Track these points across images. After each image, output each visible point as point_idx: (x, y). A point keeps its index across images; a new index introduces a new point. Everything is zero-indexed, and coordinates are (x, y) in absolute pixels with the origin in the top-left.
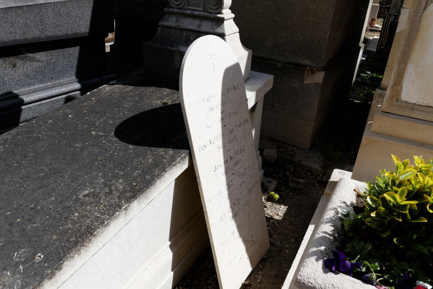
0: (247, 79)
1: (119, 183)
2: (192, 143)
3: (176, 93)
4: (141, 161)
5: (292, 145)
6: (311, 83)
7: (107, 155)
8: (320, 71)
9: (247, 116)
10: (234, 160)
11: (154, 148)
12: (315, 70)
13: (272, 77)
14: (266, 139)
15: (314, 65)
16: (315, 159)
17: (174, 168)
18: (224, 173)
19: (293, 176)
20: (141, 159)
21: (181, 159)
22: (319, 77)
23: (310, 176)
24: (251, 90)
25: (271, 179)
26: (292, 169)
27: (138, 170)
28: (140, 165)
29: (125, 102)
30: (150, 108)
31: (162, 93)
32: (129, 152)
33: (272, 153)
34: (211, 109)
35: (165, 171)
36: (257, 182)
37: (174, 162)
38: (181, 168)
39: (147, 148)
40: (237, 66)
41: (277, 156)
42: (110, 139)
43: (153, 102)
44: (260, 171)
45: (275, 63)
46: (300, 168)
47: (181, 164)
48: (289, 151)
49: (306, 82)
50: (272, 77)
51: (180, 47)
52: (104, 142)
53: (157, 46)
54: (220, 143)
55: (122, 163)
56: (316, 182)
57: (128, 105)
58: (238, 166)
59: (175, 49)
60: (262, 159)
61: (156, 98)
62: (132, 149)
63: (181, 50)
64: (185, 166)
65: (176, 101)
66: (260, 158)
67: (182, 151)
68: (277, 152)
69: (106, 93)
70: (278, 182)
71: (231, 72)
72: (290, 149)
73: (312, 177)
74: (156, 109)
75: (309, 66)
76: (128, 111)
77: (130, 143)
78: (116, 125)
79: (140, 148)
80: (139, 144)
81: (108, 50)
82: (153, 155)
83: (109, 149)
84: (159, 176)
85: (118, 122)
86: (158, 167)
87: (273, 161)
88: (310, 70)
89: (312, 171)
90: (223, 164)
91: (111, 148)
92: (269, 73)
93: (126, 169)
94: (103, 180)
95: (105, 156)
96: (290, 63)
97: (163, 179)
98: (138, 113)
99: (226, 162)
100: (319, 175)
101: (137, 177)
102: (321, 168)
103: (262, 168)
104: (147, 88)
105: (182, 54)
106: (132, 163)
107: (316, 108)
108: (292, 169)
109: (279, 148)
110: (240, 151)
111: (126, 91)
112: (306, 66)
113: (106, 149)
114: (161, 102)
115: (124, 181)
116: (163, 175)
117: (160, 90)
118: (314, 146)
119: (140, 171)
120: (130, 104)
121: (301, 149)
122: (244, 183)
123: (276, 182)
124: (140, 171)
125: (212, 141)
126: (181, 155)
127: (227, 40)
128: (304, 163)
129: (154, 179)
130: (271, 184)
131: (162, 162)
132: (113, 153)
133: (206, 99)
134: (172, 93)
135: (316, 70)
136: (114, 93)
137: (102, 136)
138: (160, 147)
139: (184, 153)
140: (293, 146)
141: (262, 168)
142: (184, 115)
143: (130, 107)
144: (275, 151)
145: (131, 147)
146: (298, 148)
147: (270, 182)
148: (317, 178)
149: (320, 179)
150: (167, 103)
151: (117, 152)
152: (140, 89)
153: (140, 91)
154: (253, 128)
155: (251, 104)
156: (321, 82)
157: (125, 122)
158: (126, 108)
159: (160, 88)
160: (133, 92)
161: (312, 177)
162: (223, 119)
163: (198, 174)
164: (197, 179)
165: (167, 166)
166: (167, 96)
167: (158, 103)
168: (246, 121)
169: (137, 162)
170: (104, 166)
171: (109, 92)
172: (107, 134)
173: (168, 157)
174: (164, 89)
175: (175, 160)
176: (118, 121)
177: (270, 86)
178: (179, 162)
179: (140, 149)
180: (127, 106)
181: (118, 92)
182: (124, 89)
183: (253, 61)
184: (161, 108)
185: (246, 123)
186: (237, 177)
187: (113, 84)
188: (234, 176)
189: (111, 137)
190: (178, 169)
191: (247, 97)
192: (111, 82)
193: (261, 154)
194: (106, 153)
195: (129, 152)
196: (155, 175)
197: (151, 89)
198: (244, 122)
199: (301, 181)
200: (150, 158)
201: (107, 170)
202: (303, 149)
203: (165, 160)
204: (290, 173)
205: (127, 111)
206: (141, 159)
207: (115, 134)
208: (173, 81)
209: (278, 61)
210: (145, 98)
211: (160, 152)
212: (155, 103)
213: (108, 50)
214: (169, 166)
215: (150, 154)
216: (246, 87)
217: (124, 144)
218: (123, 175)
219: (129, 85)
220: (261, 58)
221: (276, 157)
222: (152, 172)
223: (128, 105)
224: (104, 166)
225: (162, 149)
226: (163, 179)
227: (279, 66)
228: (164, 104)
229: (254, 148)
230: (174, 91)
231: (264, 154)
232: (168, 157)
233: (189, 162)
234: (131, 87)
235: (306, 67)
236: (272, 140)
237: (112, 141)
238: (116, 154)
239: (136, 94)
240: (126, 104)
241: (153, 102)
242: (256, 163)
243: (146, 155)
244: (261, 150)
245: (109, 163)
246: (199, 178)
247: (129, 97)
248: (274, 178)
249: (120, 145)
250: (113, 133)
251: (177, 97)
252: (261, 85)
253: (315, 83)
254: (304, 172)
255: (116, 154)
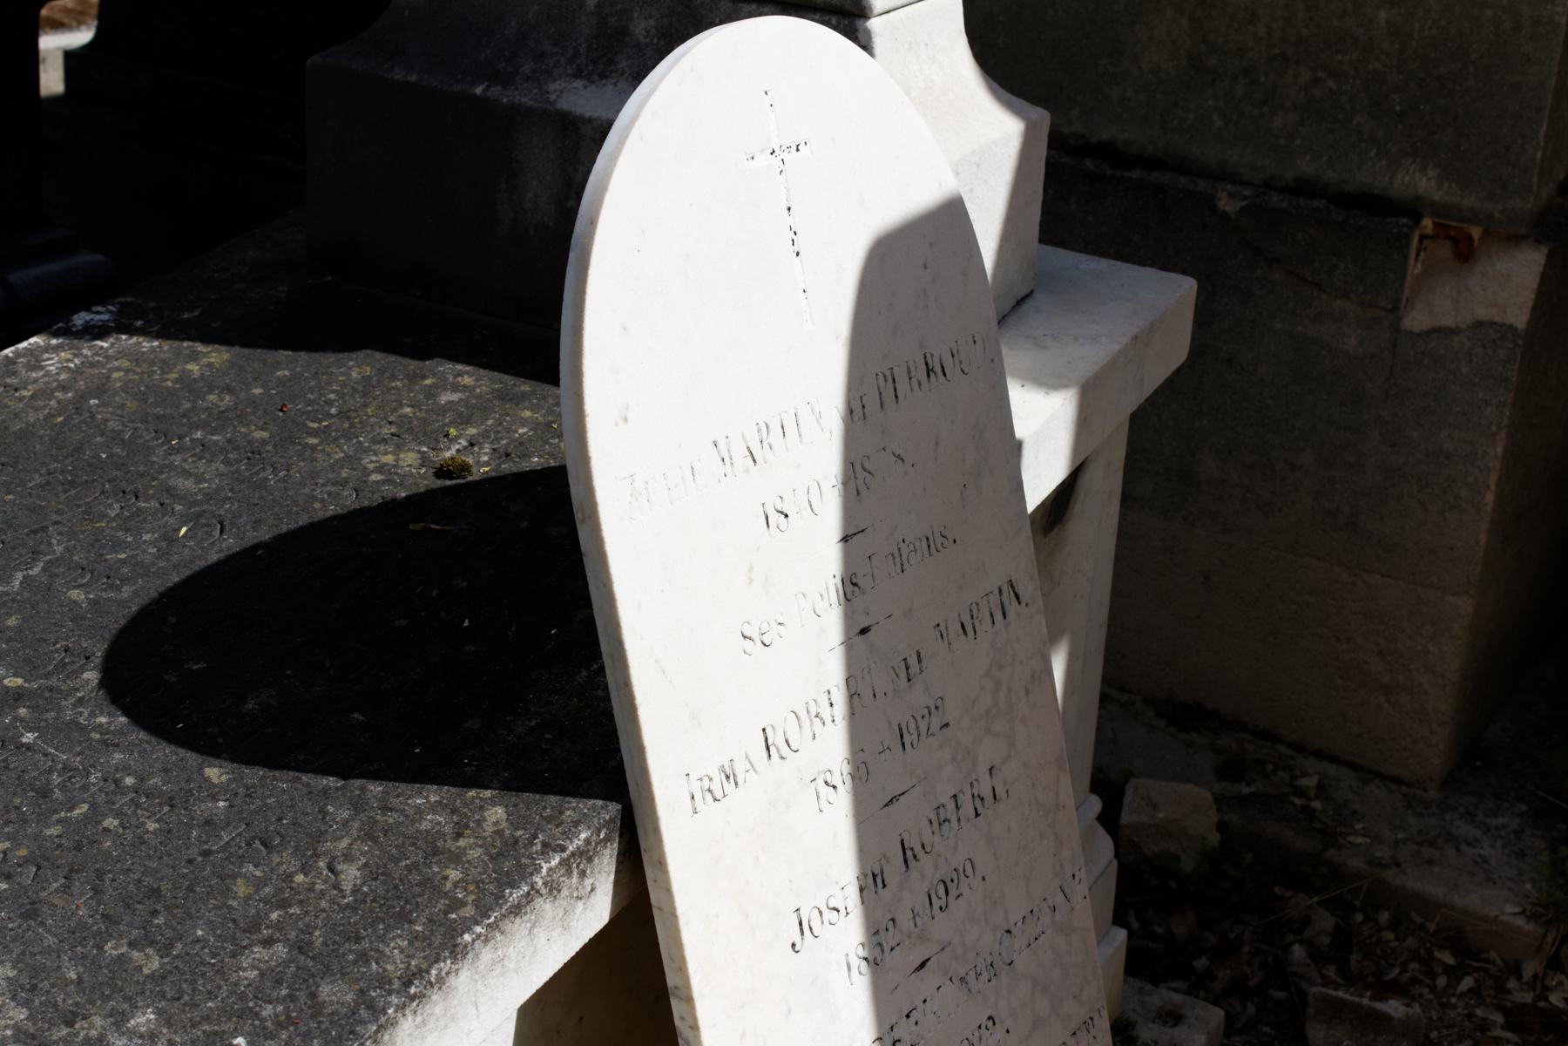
0: (1017, 303)
1: (132, 1034)
2: (640, 750)
3: (524, 397)
4: (288, 877)
5: (1320, 755)
6: (1447, 321)
7: (54, 831)
8: (1515, 240)
9: (1016, 558)
10: (928, 870)
11: (376, 788)
12: (1476, 233)
13: (1179, 291)
14: (1146, 710)
15: (1470, 201)
16: (1486, 851)
17: (518, 927)
18: (856, 963)
19: (1331, 971)
20: (285, 861)
21: (565, 863)
22: (1509, 285)
23: (1455, 974)
24: (1047, 381)
25: (1178, 998)
26: (1325, 922)
27: (268, 943)
28: (283, 904)
29: (177, 460)
30: (350, 501)
31: (431, 394)
32: (203, 809)
33: (1183, 806)
34: (775, 518)
35: (457, 952)
36: (1088, 1024)
37: (514, 885)
38: (557, 930)
39: (331, 782)
40: (949, 218)
41: (1222, 827)
42: (68, 715)
43: (369, 461)
44: (1102, 938)
45: (1201, 185)
46: (1384, 917)
47: (562, 902)
48: (1300, 792)
49: (1416, 320)
50: (1179, 291)
51: (555, 86)
52: (29, 737)
53: (398, 75)
54: (830, 748)
55: (155, 893)
56: (1499, 1018)
57: (197, 477)
58: (958, 908)
59: (522, 96)
60: (1117, 856)
61: (396, 428)
62: (225, 788)
63: (564, 104)
64: (591, 912)
65: (526, 456)
66: (1105, 845)
67: (575, 807)
68: (1219, 800)
69: (46, 393)
70: (1229, 1018)
71: (911, 267)
72: (1310, 782)
73: (1467, 982)
74: (391, 507)
75: (1438, 210)
76: (195, 519)
77: (211, 749)
78: (116, 621)
79: (282, 781)
80: (274, 759)
81: (52, 81)
82: (369, 836)
83: (63, 788)
84: (414, 986)
85: (132, 596)
86: (404, 918)
87: (1188, 864)
88: (1441, 231)
89: (1464, 943)
90: (850, 897)
91: (78, 782)
92: (1164, 262)
93: (180, 937)
94: (21, 1014)
95: (36, 837)
96: (1305, 188)
97: (437, 1005)
98: (265, 534)
99: (872, 882)
100: (1516, 970)
101: (260, 995)
102: (1533, 917)
103: (1119, 919)
104: (328, 359)
105: (582, 142)
106: (227, 892)
107: (1490, 498)
108: (1325, 922)
109: (1230, 769)
110: (966, 801)
111: (184, 377)
112: (1412, 210)
113: (45, 793)
114: (424, 461)
115: (166, 1019)
116: (441, 981)
117: (413, 378)
118: (1477, 762)
119: (281, 950)
120: (213, 472)
121: (1384, 778)
122: (999, 1033)
123: (1219, 1013)
124: (281, 950)
125: (776, 739)
126: (569, 835)
127: (878, 43)
128: (1413, 880)
129: (376, 1011)
130: (1179, 1032)
131: (432, 887)
132: (94, 816)
133: (739, 453)
134: (502, 396)
135: (1486, 233)
136: (100, 390)
137: (18, 696)
138: (420, 775)
139: (587, 823)
140: (1333, 759)
141: (1119, 919)
142: (588, 562)
143: (208, 496)
144: (1202, 795)
145: (215, 773)
146: (1367, 773)
147: (1173, 1017)
148: (1502, 990)
149: (1528, 997)
150: (465, 468)
151: (119, 814)
152: (277, 365)
153: (282, 382)
154: (1053, 638)
155: (1041, 477)
156: (1519, 317)
157: (172, 598)
158: (182, 498)
159: (414, 365)
160: (229, 390)
161: (1467, 982)
162: (851, 586)
163: (682, 969)
164: (676, 1007)
165: (469, 911)
166: (463, 421)
167: (403, 467)
168: (1007, 595)
169: (259, 884)
170: (31, 913)
171: (64, 388)
172: (53, 682)
173: (475, 854)
174: (446, 368)
175: (523, 873)
176: (127, 591)
177: (1174, 351)
178: (553, 889)
179: (280, 788)
180: (188, 485)
181: (125, 389)
182: (166, 366)
183: (1053, 173)
184: (420, 503)
185: (1012, 607)
186: (948, 988)
187: (100, 332)
188: (931, 977)
189: (80, 701)
190: (541, 934)
191: (1020, 431)
192: (80, 319)
193: (1109, 819)
194: (43, 819)
195: (203, 809)
196: (383, 981)
197: (357, 367)
198: (994, 599)
199: (1394, 1008)
200: (348, 857)
201: (51, 940)
202: (1398, 781)
203: (454, 874)
204: (1316, 955)
205: (181, 529)
206: (285, 861)
207: (103, 683)
208: (526, 325)
209: (1224, 175)
210: (314, 433)
211: (420, 812)
212: (380, 469)
213: (52, 81)
214: (483, 912)
215: (351, 830)
216: (1011, 357)
217: (165, 752)
218: (159, 977)
219: (206, 340)
220: (1106, 151)
221: (1214, 838)
222: (364, 958)
223: (199, 479)
224: (31, 913)
225: (434, 794)
226: (438, 1010)
227: (1226, 205)
228: (442, 472)
229: (1066, 782)
230: (509, 380)
231: (1126, 818)
232: (475, 854)
233: (617, 884)
234: (216, 356)
235: (1417, 218)
236: (1186, 715)
237: (83, 729)
238: (111, 822)
239: (253, 402)
240: (186, 474)
241: (369, 461)
242: (1080, 890)
243: (320, 836)
244: (1107, 786)
245: (66, 889)
246: (689, 1000)
247: (203, 425)
248: (1199, 986)
249: (140, 758)
250: (92, 676)
251: (535, 426)
252: (1116, 347)
253: (1479, 324)
254: (1411, 942)
255: (111, 822)
